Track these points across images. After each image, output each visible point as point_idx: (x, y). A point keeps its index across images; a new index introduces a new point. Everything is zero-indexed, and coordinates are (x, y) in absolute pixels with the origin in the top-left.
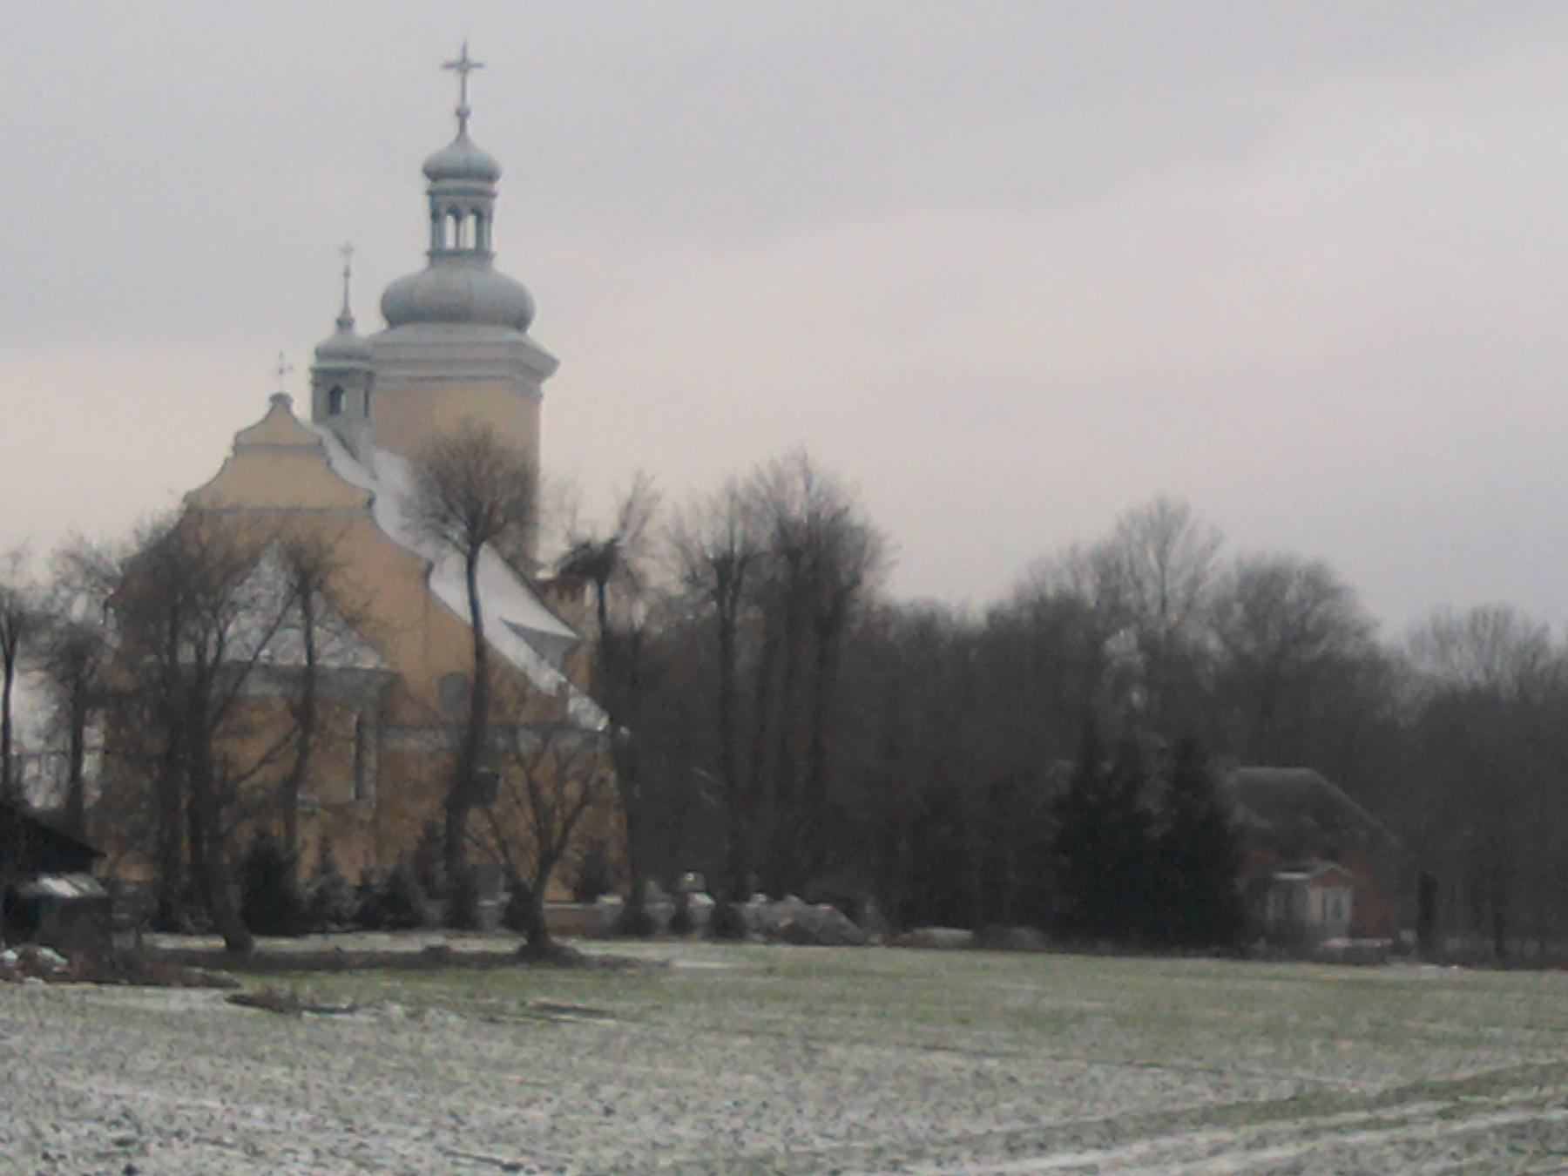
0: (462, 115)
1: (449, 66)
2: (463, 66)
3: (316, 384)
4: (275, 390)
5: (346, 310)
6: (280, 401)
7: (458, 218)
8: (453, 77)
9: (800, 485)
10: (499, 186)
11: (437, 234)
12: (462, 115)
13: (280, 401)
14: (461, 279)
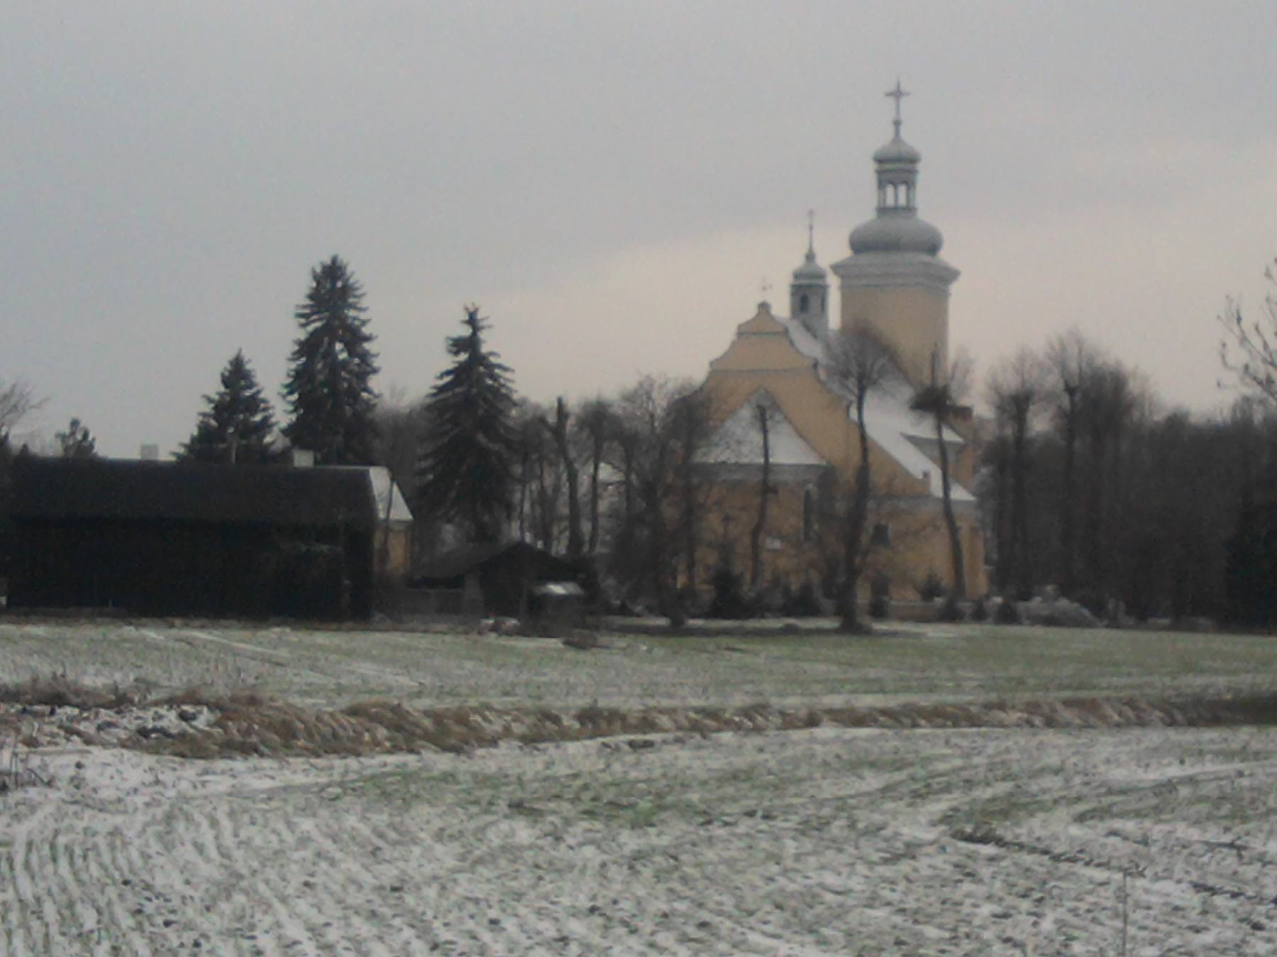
0: (897, 124)
1: (889, 94)
2: (897, 94)
3: (793, 294)
4: (760, 300)
5: (811, 249)
6: (764, 307)
7: (895, 186)
8: (891, 100)
9: (1076, 350)
10: (920, 166)
11: (882, 197)
12: (897, 124)
13: (764, 307)
14: (897, 225)
